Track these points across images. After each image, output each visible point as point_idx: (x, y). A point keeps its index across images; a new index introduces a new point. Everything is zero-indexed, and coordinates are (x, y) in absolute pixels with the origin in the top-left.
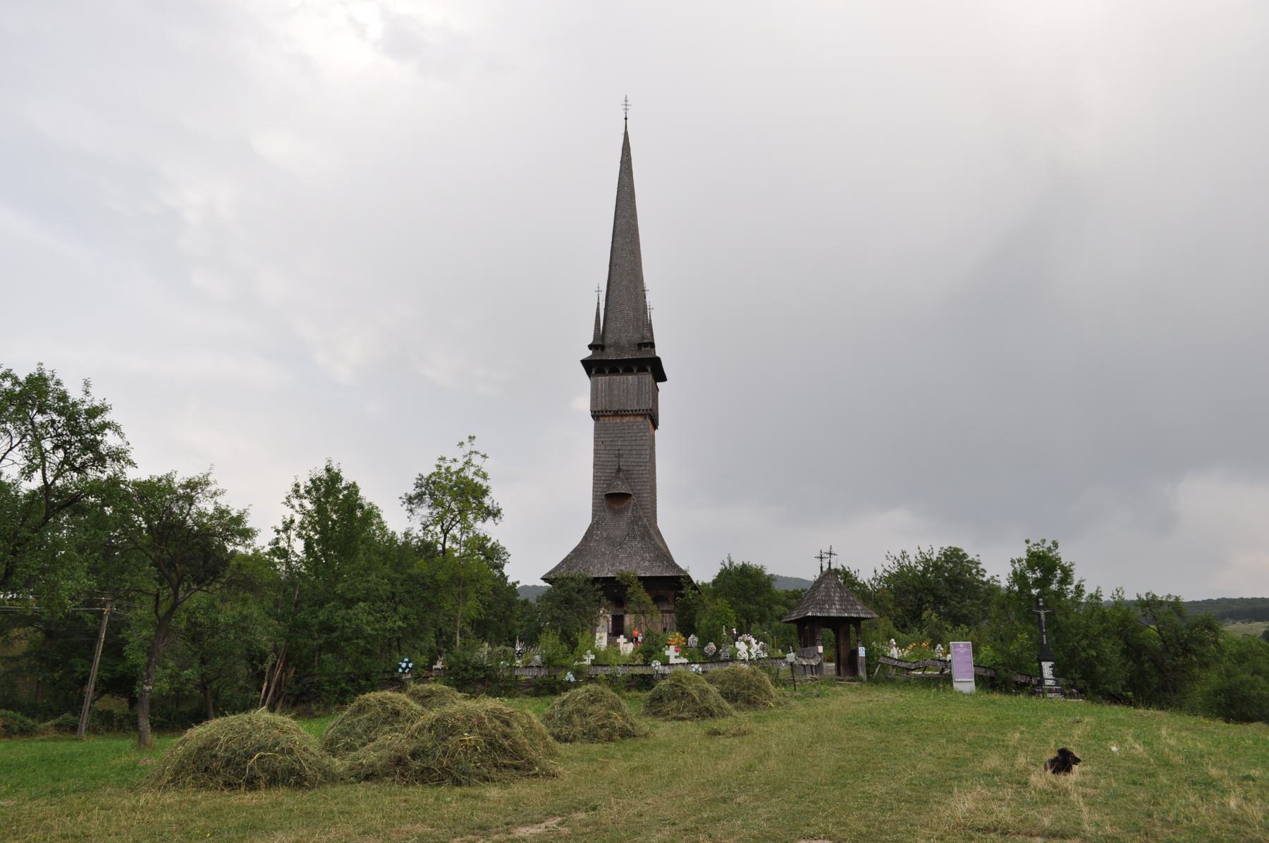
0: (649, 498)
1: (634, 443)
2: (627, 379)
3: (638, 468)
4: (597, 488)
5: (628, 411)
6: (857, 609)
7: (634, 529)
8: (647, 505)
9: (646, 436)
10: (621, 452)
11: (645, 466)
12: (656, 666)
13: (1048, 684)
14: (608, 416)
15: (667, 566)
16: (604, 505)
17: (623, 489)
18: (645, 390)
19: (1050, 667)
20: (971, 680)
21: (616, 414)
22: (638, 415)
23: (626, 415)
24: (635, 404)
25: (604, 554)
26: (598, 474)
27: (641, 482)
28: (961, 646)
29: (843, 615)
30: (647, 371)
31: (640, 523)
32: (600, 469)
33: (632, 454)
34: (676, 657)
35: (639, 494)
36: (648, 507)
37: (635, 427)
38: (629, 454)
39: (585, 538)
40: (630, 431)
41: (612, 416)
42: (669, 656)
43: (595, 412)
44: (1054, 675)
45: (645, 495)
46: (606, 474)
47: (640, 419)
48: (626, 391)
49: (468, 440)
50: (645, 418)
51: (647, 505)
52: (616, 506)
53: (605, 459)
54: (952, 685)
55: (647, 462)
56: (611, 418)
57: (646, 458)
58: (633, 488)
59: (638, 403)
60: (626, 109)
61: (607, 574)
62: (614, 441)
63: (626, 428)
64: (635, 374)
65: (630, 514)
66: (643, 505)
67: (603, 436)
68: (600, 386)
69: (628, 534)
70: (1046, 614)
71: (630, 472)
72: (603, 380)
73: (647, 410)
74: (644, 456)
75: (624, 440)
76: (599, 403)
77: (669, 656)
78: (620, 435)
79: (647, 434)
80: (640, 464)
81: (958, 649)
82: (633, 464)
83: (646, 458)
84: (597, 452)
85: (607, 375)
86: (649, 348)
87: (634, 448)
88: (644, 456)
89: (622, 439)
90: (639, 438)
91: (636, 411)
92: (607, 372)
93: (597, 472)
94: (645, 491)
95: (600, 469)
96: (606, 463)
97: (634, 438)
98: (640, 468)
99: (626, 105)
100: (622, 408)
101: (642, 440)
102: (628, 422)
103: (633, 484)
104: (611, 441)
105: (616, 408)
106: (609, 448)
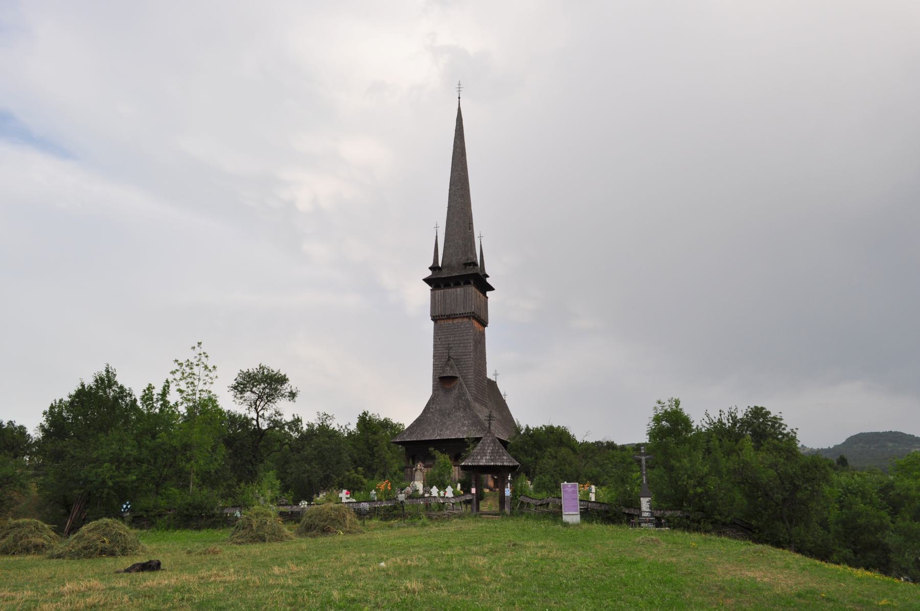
0: (472, 380)
1: (461, 338)
2: (456, 291)
3: (464, 357)
4: (436, 373)
5: (457, 314)
6: (503, 459)
7: (459, 403)
8: (471, 384)
9: (470, 332)
10: (450, 346)
11: (470, 355)
12: (302, 505)
13: (645, 515)
14: (443, 319)
15: (480, 430)
16: (439, 385)
17: (449, 373)
18: (469, 298)
19: (648, 502)
20: (576, 513)
21: (449, 317)
22: (464, 317)
23: (456, 318)
24: (462, 310)
25: (436, 422)
26: (437, 363)
27: (467, 367)
28: (569, 486)
29: (490, 464)
30: (470, 283)
31: (463, 398)
32: (438, 359)
33: (461, 347)
34: (347, 498)
35: (465, 376)
36: (472, 385)
37: (462, 326)
38: (459, 347)
39: (424, 411)
40: (459, 329)
41: (446, 319)
42: (341, 498)
43: (434, 317)
44: (650, 508)
45: (470, 377)
46: (442, 363)
47: (466, 320)
48: (455, 300)
49: (197, 345)
50: (470, 319)
51: (471, 384)
52: (447, 387)
53: (441, 352)
54: (562, 517)
55: (471, 352)
56: (446, 321)
57: (470, 349)
58: (460, 372)
59: (464, 308)
60: (459, 91)
61: (436, 437)
62: (448, 337)
63: (456, 327)
64: (462, 287)
65: (456, 391)
66: (468, 384)
67: (440, 334)
68: (437, 298)
69: (454, 407)
70: (646, 459)
71: (459, 360)
72: (439, 292)
73: (470, 313)
74: (469, 348)
75: (455, 337)
76: (437, 310)
77: (341, 498)
78: (451, 333)
79: (471, 331)
80: (466, 354)
81: (567, 489)
82: (461, 354)
83: (470, 349)
84: (435, 346)
85: (442, 289)
86: (472, 267)
87: (462, 342)
88: (469, 348)
89: (453, 336)
90: (465, 334)
91: (463, 314)
92: (442, 287)
93: (436, 361)
94: (470, 374)
95: (438, 359)
96: (442, 354)
97: (461, 335)
98: (466, 357)
99: (459, 88)
100: (452, 313)
101: (468, 335)
102: (457, 323)
103: (461, 369)
104: (446, 338)
105: (448, 313)
106: (444, 343)
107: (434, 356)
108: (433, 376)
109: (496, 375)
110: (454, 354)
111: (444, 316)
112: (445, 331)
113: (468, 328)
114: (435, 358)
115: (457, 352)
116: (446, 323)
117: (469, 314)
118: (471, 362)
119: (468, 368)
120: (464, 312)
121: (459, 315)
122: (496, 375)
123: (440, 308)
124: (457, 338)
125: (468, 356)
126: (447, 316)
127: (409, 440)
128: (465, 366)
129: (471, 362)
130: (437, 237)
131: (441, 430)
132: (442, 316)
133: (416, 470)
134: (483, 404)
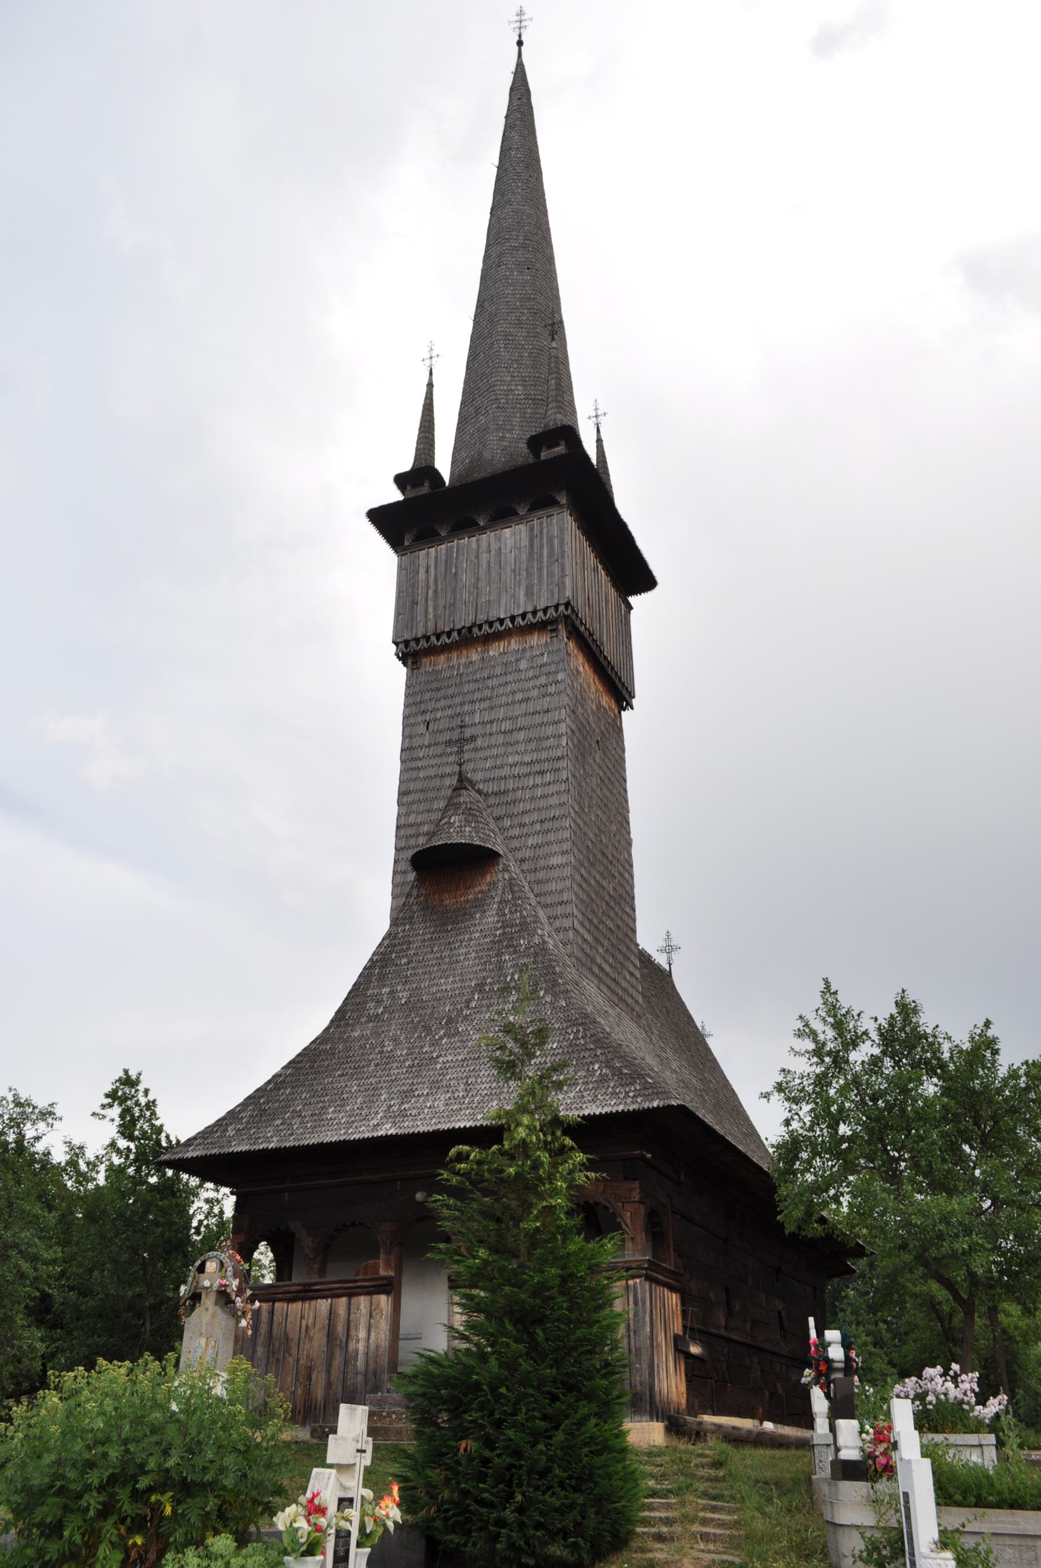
5: (501, 621)
15: (603, 1080)
23: (498, 636)
25: (389, 1059)
26: (412, 819)
37: (523, 665)
38: (508, 744)
39: (340, 1015)
43: (406, 643)
47: (536, 640)
53: (432, 772)
56: (455, 655)
59: (529, 594)
69: (480, 987)
72: (429, 556)
73: (556, 607)
76: (420, 617)
78: (477, 695)
79: (560, 676)
82: (516, 771)
88: (551, 742)
90: (535, 693)
91: (523, 616)
93: (408, 814)
97: (519, 696)
98: (538, 780)
100: (482, 618)
105: (464, 619)
107: (402, 794)
108: (395, 873)
109: (669, 949)
110: (488, 775)
111: (449, 634)
112: (450, 692)
113: (547, 669)
114: (409, 798)
115: (502, 767)
116: (455, 662)
117: (552, 612)
118: (564, 798)
119: (547, 825)
120: (530, 608)
121: (508, 622)
122: (669, 949)
123: (430, 610)
124: (501, 713)
125: (548, 777)
126: (459, 631)
127: (244, 1148)
128: (535, 816)
129: (564, 798)
130: (430, 385)
131: (407, 1095)
132: (438, 637)
133: (196, 1297)
134: (621, 999)
